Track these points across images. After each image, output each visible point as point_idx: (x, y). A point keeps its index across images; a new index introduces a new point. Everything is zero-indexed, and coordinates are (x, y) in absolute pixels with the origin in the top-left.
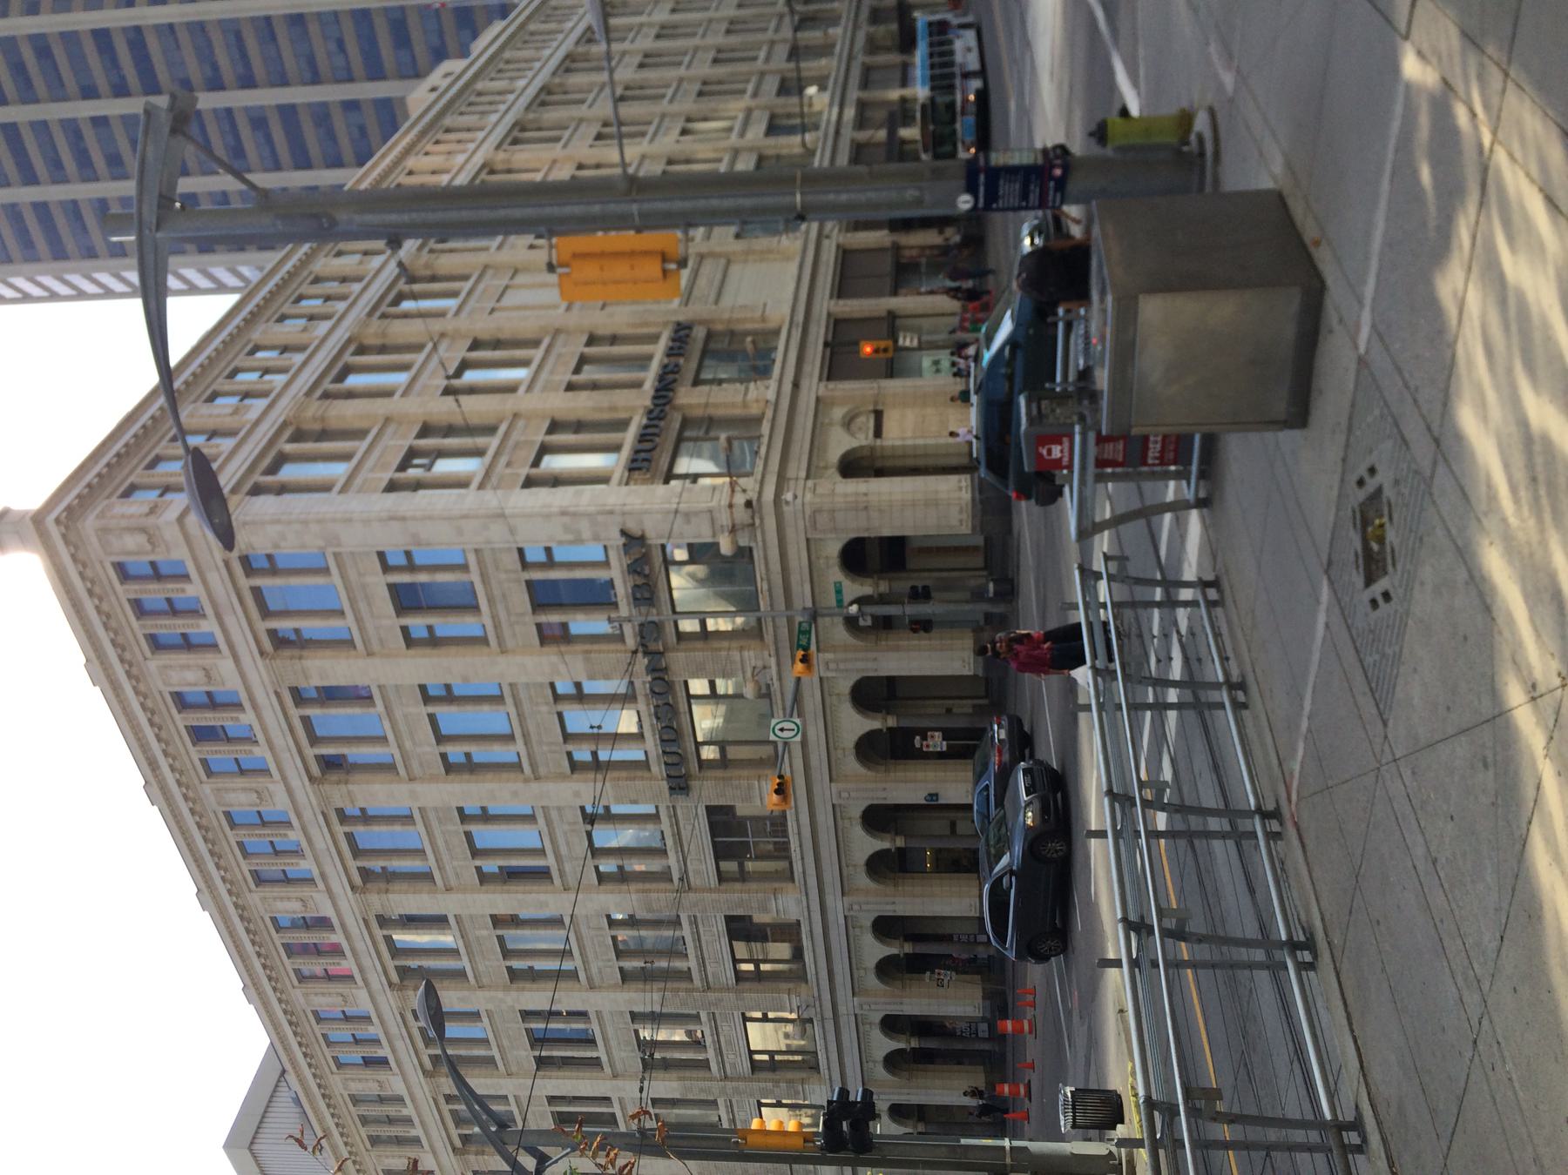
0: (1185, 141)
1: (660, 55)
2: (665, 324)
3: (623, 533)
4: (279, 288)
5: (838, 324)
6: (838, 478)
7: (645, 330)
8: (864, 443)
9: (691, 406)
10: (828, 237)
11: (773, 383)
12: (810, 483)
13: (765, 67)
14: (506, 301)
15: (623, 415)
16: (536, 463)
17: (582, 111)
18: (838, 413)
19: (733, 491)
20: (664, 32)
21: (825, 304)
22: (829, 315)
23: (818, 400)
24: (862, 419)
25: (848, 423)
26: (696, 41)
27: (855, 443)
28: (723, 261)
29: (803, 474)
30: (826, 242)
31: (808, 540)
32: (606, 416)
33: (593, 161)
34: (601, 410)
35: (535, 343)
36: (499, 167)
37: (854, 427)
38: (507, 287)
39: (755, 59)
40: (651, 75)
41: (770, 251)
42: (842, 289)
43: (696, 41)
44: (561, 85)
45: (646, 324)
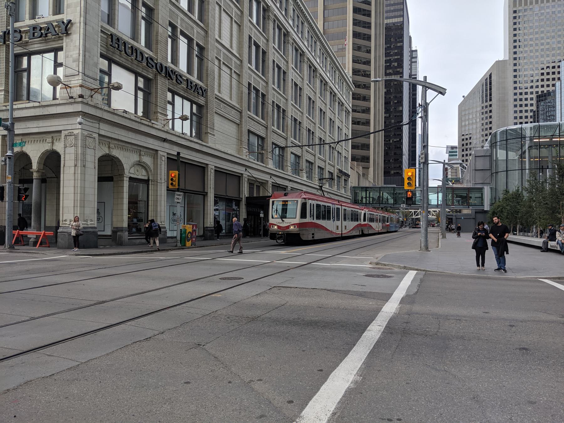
0: (543, 171)
1: (284, 80)
2: (207, 86)
3: (70, 21)
4: (327, 50)
5: (203, 168)
6: (99, 154)
7: (204, 75)
8: (126, 171)
9: (157, 84)
10: (246, 170)
11: (291, 174)
12: (96, 136)
13: (327, 163)
14: (224, 15)
15: (154, 46)
16: (183, 34)
17: (318, 95)
18: (147, 160)
19: (92, 90)
20: (332, 121)
21: (212, 164)
22: (207, 165)
23: (157, 151)
24: (144, 173)
25: (140, 164)
26: (328, 133)
27: (126, 166)
28: (238, 122)
29: (102, 133)
30: (244, 169)
31: (60, 132)
32: (154, 38)
33: (302, 94)
34: (157, 35)
35: (201, 18)
36: (286, 38)
37: (139, 168)
38: (232, 18)
39: (320, 154)
40: (305, 101)
41: (241, 144)
42: (219, 172)
43: (328, 133)
44: (316, 75)
45: (157, 43)
